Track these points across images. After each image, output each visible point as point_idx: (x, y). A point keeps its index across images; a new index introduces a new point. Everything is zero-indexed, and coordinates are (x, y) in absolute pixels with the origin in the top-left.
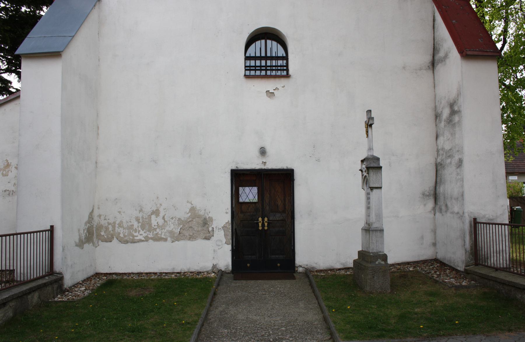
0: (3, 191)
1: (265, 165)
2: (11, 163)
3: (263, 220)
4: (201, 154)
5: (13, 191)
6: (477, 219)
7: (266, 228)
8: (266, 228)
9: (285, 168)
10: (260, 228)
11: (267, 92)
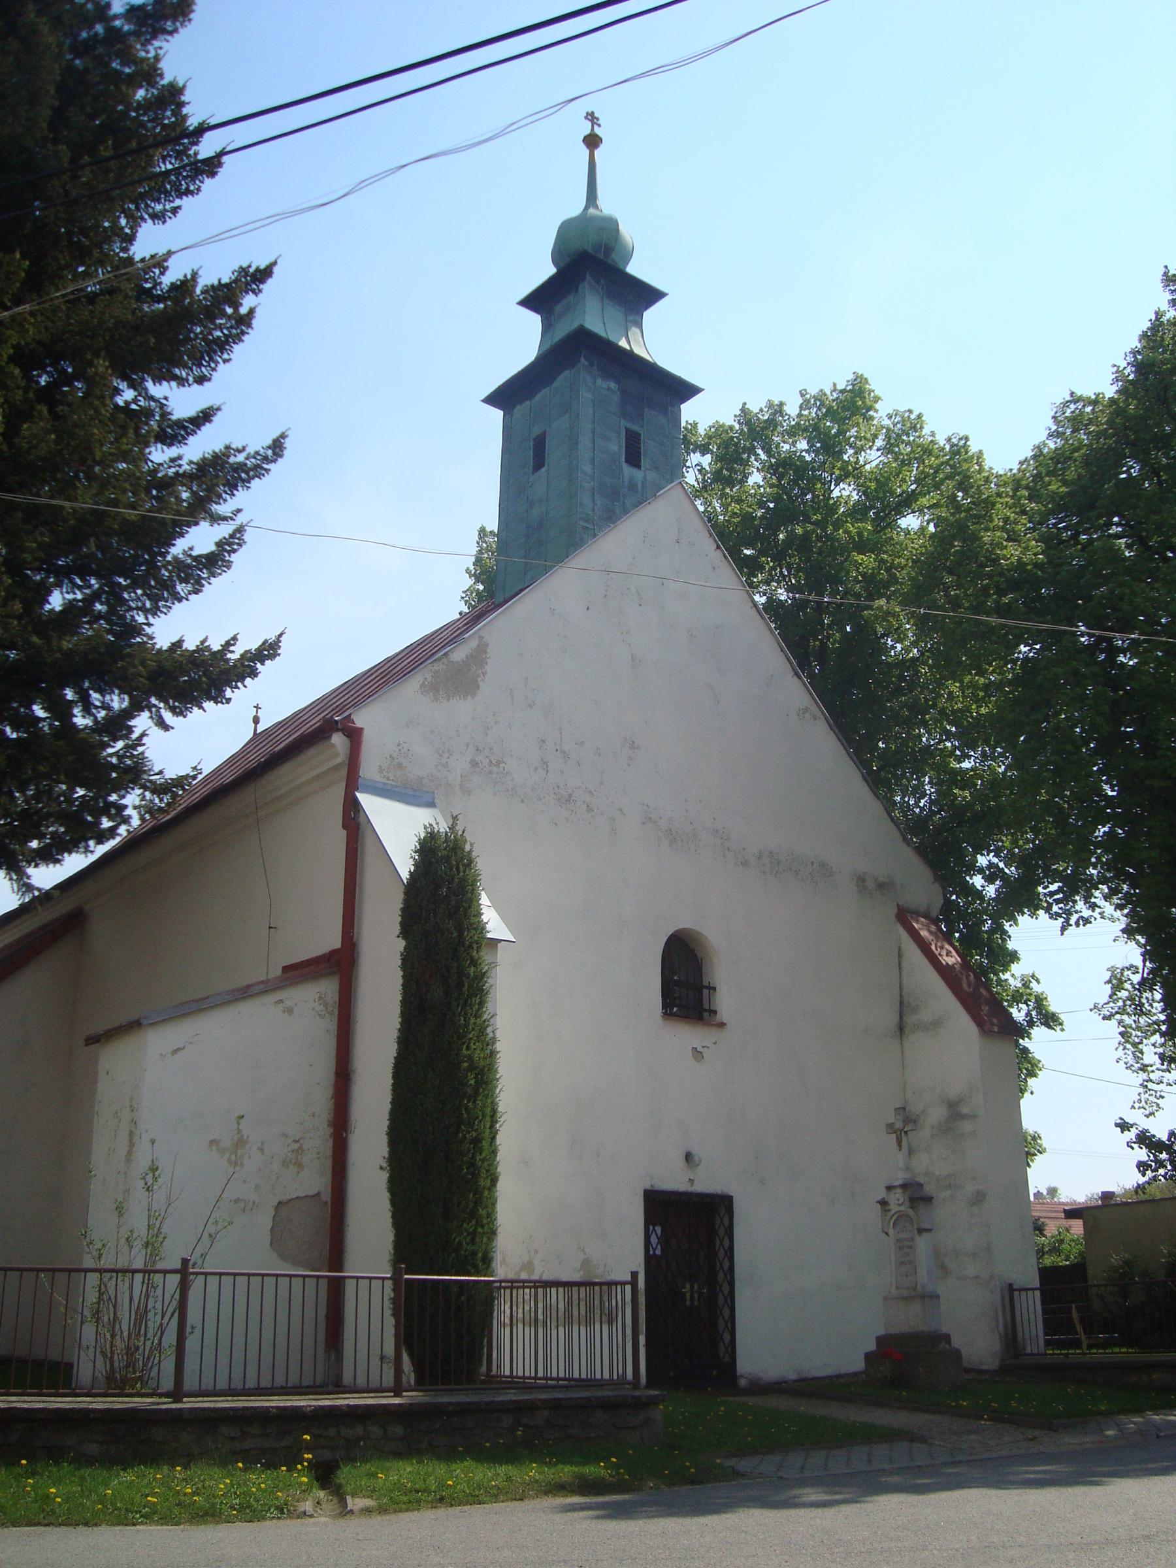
0: (231, 1201)
1: (692, 1185)
2: (248, 1137)
3: (692, 1287)
4: (598, 1156)
5: (254, 1203)
6: (878, 1334)
7: (696, 1303)
8: (696, 1303)
9: (719, 1192)
10: (688, 1303)
11: (694, 1049)
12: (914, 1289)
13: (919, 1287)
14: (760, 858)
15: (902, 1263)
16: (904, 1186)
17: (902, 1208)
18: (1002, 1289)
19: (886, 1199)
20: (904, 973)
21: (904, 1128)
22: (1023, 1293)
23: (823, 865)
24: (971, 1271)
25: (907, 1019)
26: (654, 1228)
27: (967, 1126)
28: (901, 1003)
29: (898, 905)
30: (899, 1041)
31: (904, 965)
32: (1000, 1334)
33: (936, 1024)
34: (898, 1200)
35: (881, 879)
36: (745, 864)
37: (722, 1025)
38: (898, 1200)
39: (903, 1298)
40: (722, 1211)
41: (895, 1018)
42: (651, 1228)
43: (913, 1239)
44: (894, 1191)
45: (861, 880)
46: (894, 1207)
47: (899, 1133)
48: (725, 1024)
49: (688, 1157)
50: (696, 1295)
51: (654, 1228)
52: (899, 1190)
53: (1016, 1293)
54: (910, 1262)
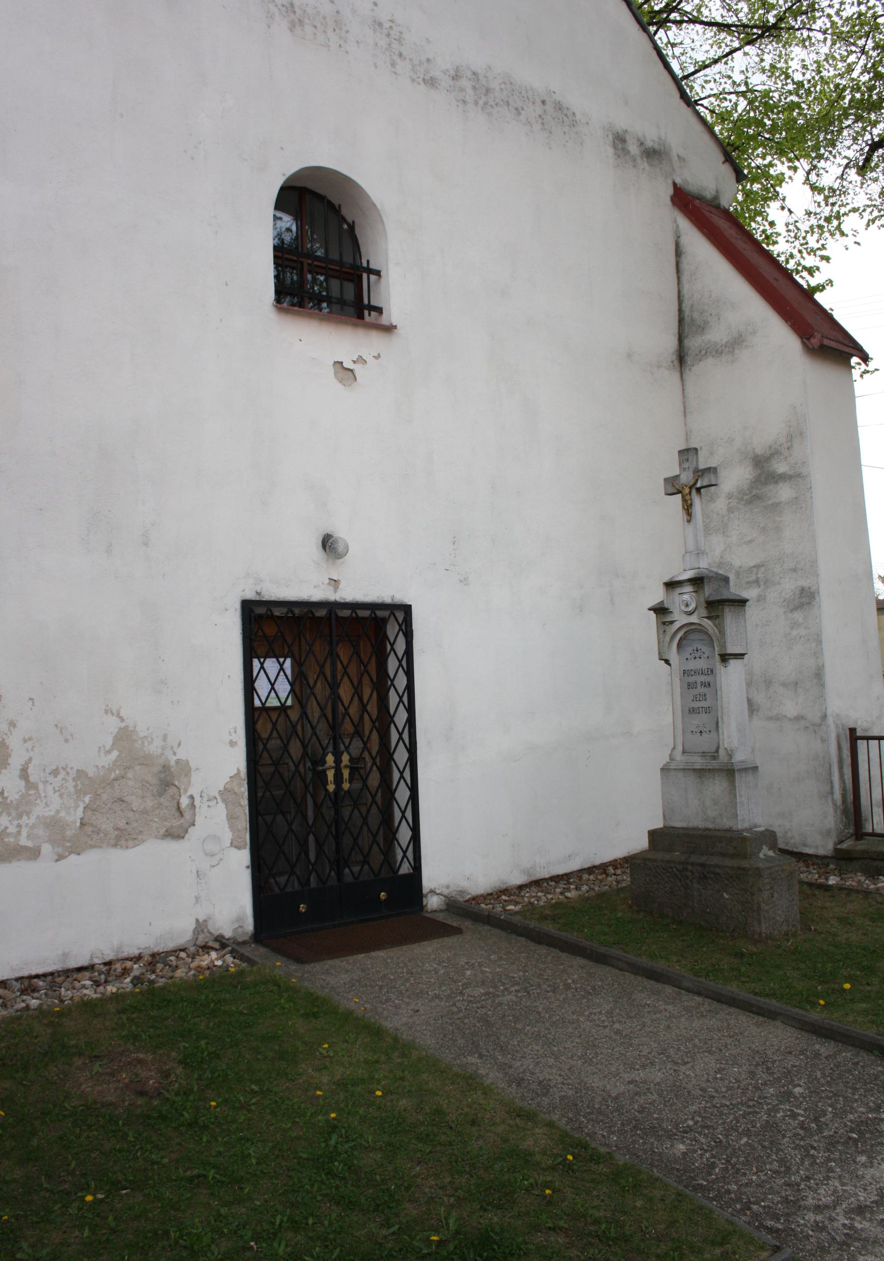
3: (338, 761)
7: (346, 786)
10: (331, 787)
12: (715, 755)
13: (721, 752)
14: (456, 77)
15: (692, 711)
16: (697, 582)
17: (694, 619)
18: (838, 737)
19: (666, 606)
20: (685, 278)
21: (696, 483)
22: (874, 743)
23: (559, 107)
24: (790, 708)
25: (689, 343)
26: (262, 664)
27: (784, 492)
28: (681, 321)
29: (675, 184)
30: (678, 375)
31: (685, 265)
32: (835, 804)
33: (737, 343)
34: (687, 605)
35: (649, 144)
36: (431, 83)
37: (389, 329)
38: (687, 605)
39: (695, 770)
40: (392, 630)
41: (671, 343)
42: (256, 663)
43: (712, 671)
44: (679, 590)
45: (619, 140)
46: (680, 619)
47: (687, 490)
48: (395, 327)
49: (328, 543)
50: (346, 773)
51: (262, 664)
52: (688, 588)
53: (862, 745)
54: (708, 710)
